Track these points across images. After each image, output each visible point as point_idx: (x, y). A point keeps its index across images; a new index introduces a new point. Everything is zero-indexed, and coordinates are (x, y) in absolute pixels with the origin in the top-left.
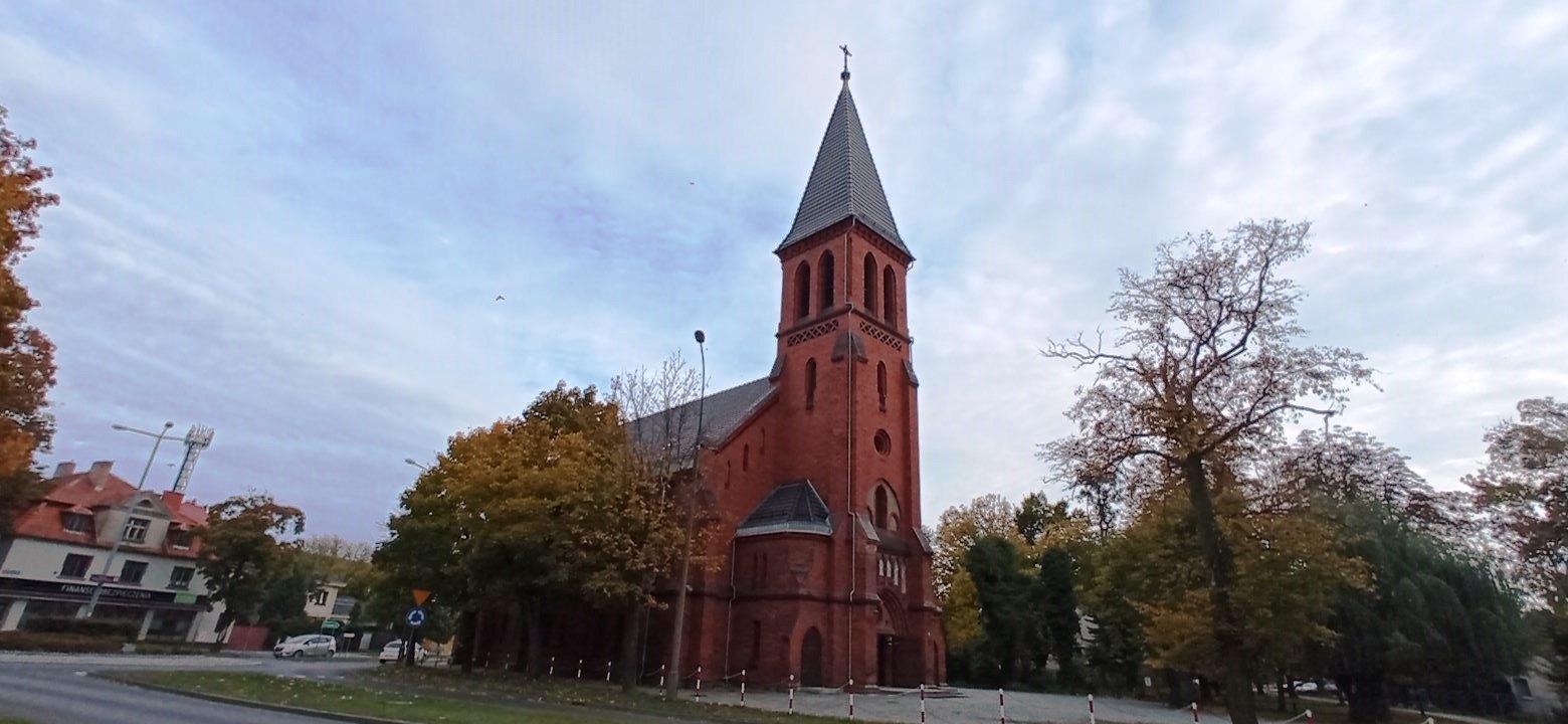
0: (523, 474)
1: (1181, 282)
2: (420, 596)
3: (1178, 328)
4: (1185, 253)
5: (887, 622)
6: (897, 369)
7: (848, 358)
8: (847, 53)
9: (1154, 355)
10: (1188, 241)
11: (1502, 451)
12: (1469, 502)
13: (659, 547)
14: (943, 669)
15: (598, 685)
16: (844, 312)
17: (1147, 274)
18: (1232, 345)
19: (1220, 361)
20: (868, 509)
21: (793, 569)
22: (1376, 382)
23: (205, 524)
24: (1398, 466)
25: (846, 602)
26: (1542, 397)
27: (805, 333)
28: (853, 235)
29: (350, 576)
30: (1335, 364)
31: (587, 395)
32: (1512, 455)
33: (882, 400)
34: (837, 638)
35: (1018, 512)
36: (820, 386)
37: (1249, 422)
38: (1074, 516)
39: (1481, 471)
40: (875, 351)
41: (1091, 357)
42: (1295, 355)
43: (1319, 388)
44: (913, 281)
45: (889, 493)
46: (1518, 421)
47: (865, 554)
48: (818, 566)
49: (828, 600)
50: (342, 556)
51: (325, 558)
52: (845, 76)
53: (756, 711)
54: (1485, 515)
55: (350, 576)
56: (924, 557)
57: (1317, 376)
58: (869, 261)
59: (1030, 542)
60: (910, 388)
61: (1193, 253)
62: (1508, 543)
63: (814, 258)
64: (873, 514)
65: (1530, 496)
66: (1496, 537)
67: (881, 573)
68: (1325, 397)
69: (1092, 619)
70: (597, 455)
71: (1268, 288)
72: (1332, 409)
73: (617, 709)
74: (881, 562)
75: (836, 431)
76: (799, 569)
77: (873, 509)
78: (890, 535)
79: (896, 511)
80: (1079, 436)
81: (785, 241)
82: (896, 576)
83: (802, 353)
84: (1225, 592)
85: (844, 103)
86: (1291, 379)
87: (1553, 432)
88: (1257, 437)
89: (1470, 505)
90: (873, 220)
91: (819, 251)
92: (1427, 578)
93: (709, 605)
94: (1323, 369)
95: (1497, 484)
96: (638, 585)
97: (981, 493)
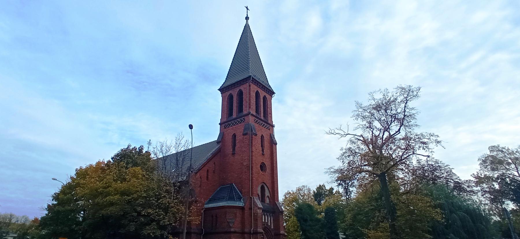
0: (114, 185)
1: (378, 108)
3: (377, 124)
4: (379, 96)
6: (268, 137)
7: (249, 133)
8: (248, 9)
9: (368, 135)
10: (380, 92)
11: (484, 164)
12: (473, 183)
17: (366, 104)
18: (396, 131)
20: (258, 195)
22: (443, 145)
24: (450, 173)
25: (250, 233)
26: (496, 145)
27: (231, 123)
28: (251, 83)
29: (18, 231)
30: (430, 139)
32: (487, 166)
33: (263, 150)
35: (314, 192)
36: (238, 145)
37: (402, 160)
38: (336, 194)
39: (477, 172)
40: (261, 131)
41: (345, 135)
42: (417, 135)
43: (424, 148)
44: (275, 103)
45: (265, 187)
46: (489, 153)
47: (257, 214)
48: (239, 219)
49: (243, 233)
50: (14, 222)
51: (5, 223)
52: (247, 18)
54: (479, 188)
55: (18, 231)
57: (424, 143)
58: (257, 94)
59: (319, 204)
61: (381, 97)
62: (487, 198)
63: (235, 93)
64: (260, 197)
65: (493, 181)
66: (482, 195)
67: (264, 221)
68: (426, 151)
69: (343, 234)
71: (407, 110)
72: (429, 155)
74: (263, 216)
75: (245, 164)
76: (230, 221)
77: (260, 195)
79: (269, 195)
81: (222, 85)
82: (269, 222)
83: (230, 131)
84: (394, 224)
85: (247, 33)
86: (415, 144)
87: (500, 157)
88: (404, 165)
89: (474, 184)
90: (258, 78)
91: (237, 90)
92: (460, 213)
94: (426, 140)
95: (483, 177)
96: (165, 231)
97: (300, 185)
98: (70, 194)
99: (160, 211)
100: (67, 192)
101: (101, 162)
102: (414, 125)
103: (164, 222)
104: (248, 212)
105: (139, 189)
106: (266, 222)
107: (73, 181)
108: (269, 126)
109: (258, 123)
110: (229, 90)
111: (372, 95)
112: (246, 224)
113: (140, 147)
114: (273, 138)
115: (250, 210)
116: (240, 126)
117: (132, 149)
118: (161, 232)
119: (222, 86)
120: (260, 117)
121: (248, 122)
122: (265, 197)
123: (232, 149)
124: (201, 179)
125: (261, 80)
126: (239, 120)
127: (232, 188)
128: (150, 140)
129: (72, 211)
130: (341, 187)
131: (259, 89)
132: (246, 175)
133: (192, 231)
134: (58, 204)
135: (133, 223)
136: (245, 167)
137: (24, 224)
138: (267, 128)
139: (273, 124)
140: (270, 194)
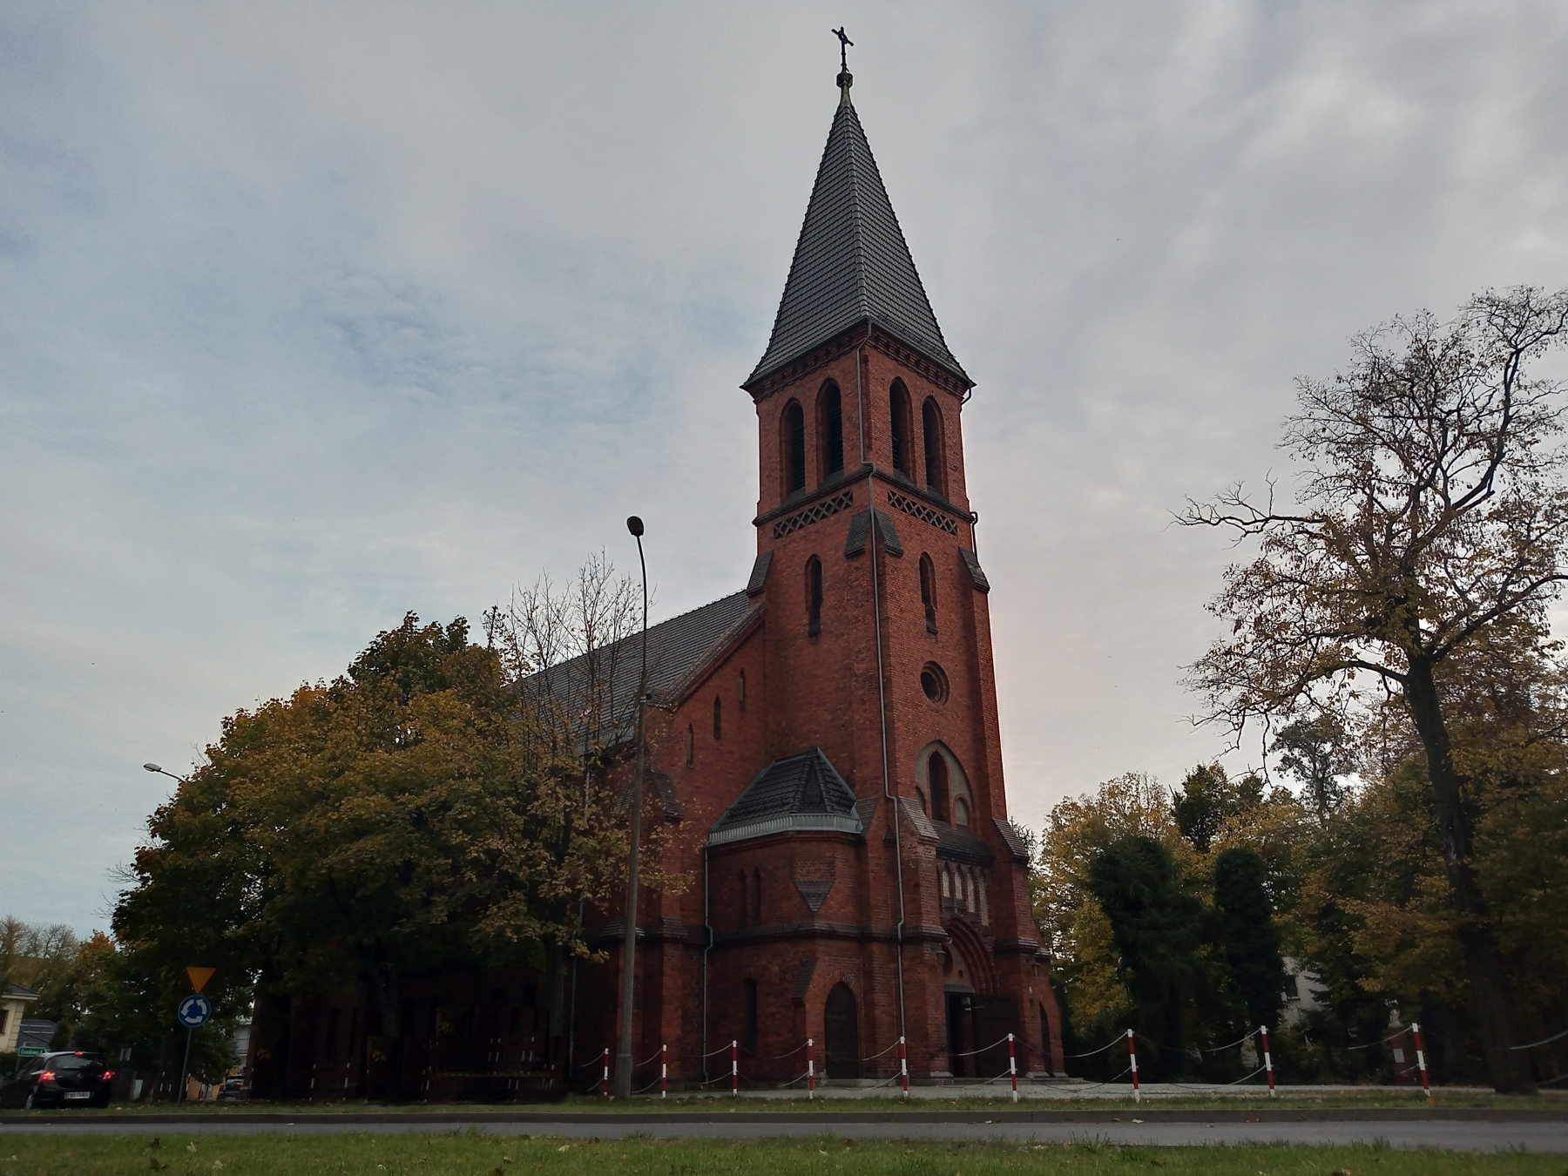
2: (199, 977)
3: (1388, 464)
5: (960, 973)
8: (844, 40)
9: (1349, 510)
10: (1396, 330)
13: (590, 859)
14: (1057, 1051)
16: (860, 478)
19: (1452, 511)
20: (918, 789)
25: (891, 940)
27: (800, 516)
28: (868, 351)
29: (39, 984)
33: (930, 615)
34: (880, 998)
36: (829, 599)
47: (917, 862)
49: (863, 939)
52: (844, 80)
55: (39, 984)
56: (1014, 866)
59: (1202, 846)
60: (976, 595)
63: (808, 394)
67: (946, 893)
70: (482, 724)
71: (1517, 394)
74: (945, 877)
75: (859, 668)
76: (811, 890)
77: (926, 789)
79: (964, 791)
80: (1231, 640)
81: (758, 367)
82: (971, 898)
83: (798, 548)
85: (845, 124)
90: (902, 320)
91: (815, 383)
93: (672, 958)
97: (1114, 773)
99: (536, 848)
100: (198, 802)
102: (1559, 460)
103: (553, 888)
104: (880, 858)
105: (451, 765)
106: (959, 900)
108: (952, 517)
109: (904, 510)
110: (783, 387)
111: (1365, 344)
112: (873, 902)
114: (971, 567)
116: (835, 523)
117: (426, 630)
119: (756, 371)
120: (910, 484)
121: (866, 503)
122: (948, 803)
123: (807, 616)
124: (692, 733)
125: (911, 327)
126: (828, 500)
129: (224, 870)
130: (1295, 772)
131: (905, 370)
132: (865, 710)
133: (667, 932)
136: (860, 679)
137: (57, 960)
138: (943, 528)
140: (970, 790)
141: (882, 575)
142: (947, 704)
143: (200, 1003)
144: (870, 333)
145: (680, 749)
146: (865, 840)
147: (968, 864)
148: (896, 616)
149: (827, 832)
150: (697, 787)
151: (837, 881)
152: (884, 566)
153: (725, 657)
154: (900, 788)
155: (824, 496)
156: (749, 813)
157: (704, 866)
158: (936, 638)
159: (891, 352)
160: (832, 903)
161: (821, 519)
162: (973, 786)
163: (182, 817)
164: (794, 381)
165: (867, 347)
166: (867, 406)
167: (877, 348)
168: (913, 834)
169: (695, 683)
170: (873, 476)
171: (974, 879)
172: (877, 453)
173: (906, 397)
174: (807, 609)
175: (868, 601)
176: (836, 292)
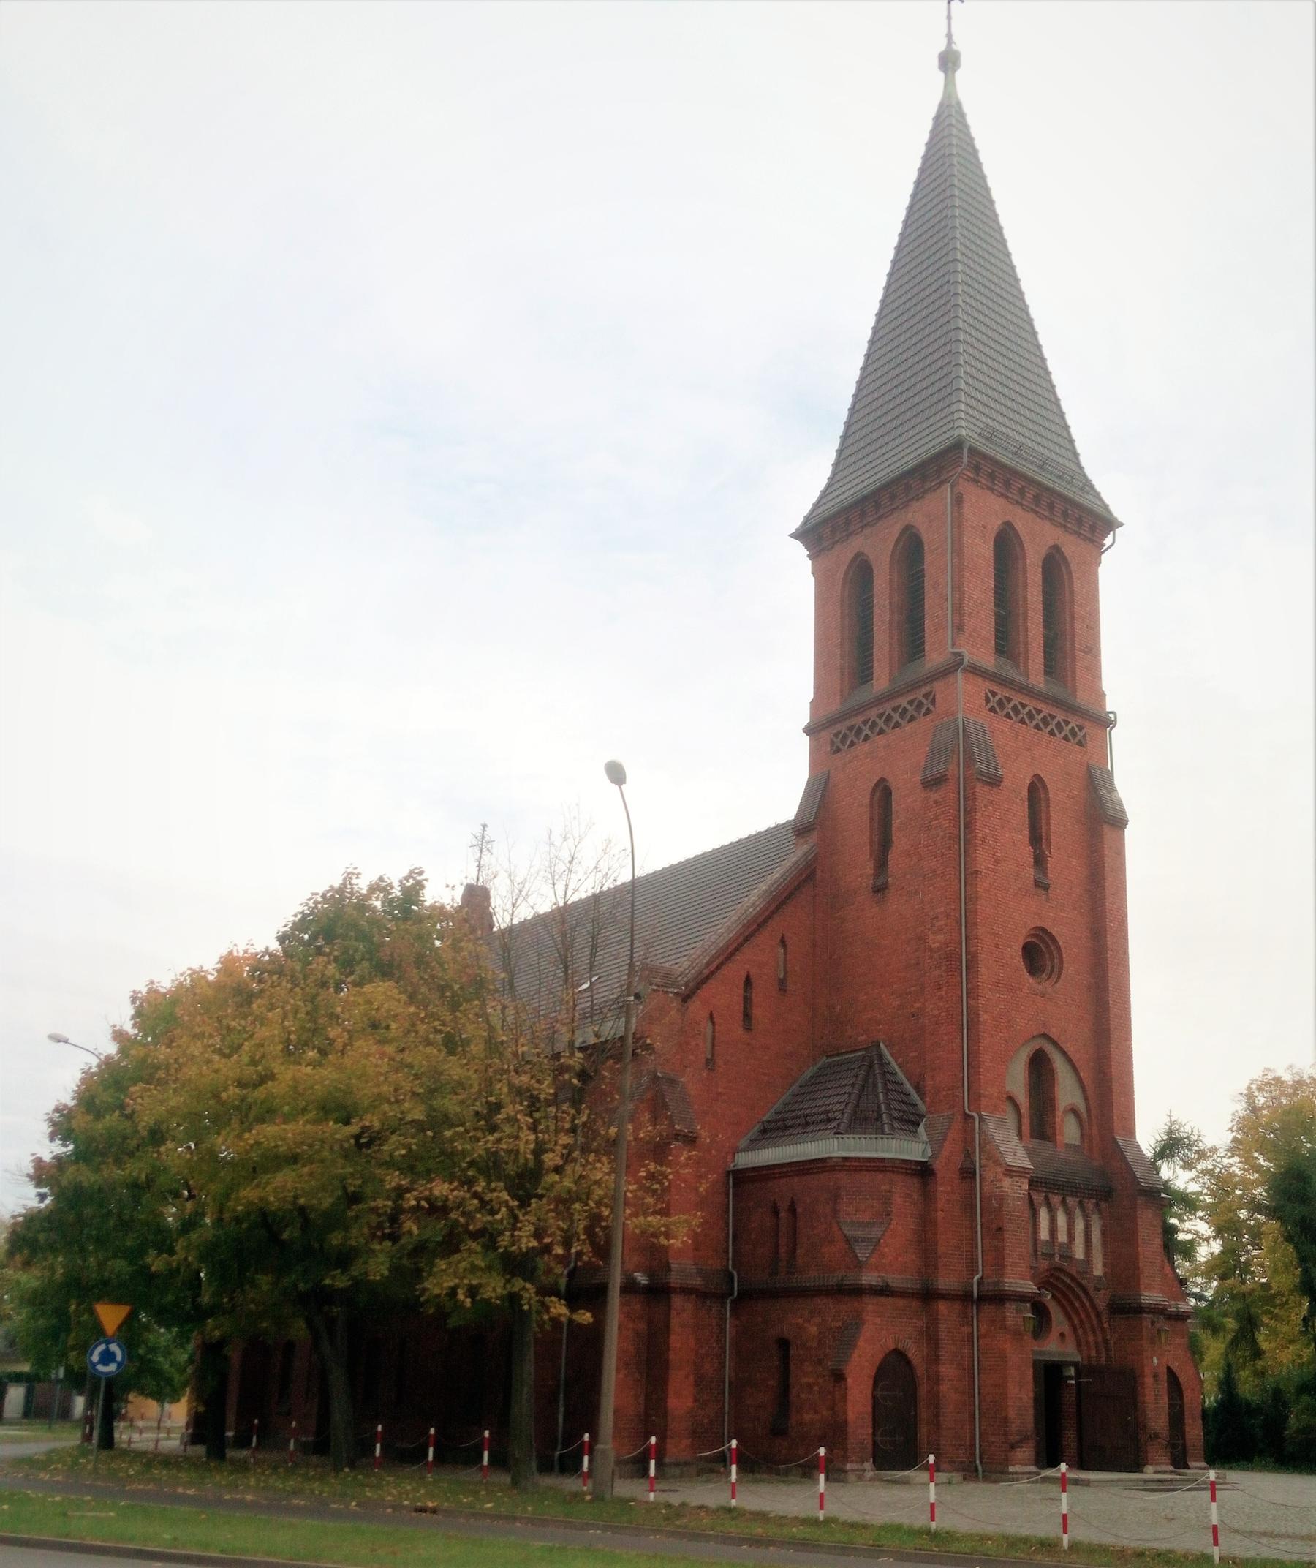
0: (286, 1074)
2: (111, 1316)
5: (1062, 1335)
13: (564, 1203)
14: (1195, 1432)
15: (470, 1475)
16: (945, 672)
20: (1011, 1099)
21: (849, 1232)
23: (184, 1400)
27: (865, 723)
31: (405, 890)
33: (1040, 861)
34: (947, 1370)
36: (901, 842)
47: (1001, 1199)
48: (901, 1228)
49: (928, 1296)
52: (949, 61)
53: (761, 1517)
56: (1140, 1200)
58: (1006, 545)
67: (1044, 1235)
73: (499, 1517)
76: (859, 1233)
78: (1061, 1152)
79: (1079, 1102)
91: (891, 530)
93: (682, 1313)
98: (117, 1113)
99: (494, 1190)
101: (241, 954)
107: (123, 1051)
108: (1079, 722)
109: (1008, 716)
112: (941, 1250)
113: (407, 878)
115: (963, 1178)
118: (508, 1286)
122: (1054, 1117)
124: (713, 1023)
126: (903, 702)
127: (872, 1065)
128: (484, 826)
131: (1018, 510)
132: (941, 998)
134: (81, 1156)
135: (380, 1244)
136: (936, 955)
138: (1066, 738)
139: (1108, 710)
140: (1086, 1099)
141: (969, 812)
142: (1057, 985)
143: (114, 1347)
144: (965, 459)
145: (697, 1045)
146: (933, 1170)
147: (1077, 1197)
148: (988, 869)
149: (883, 1160)
150: (719, 1094)
151: (894, 1222)
152: (974, 800)
153: (759, 921)
154: (984, 1101)
155: (898, 696)
156: (787, 1128)
157: (728, 1194)
158: (1047, 894)
159: (999, 487)
160: (886, 1250)
161: (893, 728)
162: (1091, 1093)
163: (80, 1122)
164: (863, 527)
165: (961, 481)
166: (959, 568)
167: (977, 482)
168: (997, 1163)
169: (717, 958)
170: (965, 670)
171: (1086, 1217)
172: (970, 636)
173: (1018, 550)
174: (871, 855)
175: (949, 848)
176: (924, 395)
